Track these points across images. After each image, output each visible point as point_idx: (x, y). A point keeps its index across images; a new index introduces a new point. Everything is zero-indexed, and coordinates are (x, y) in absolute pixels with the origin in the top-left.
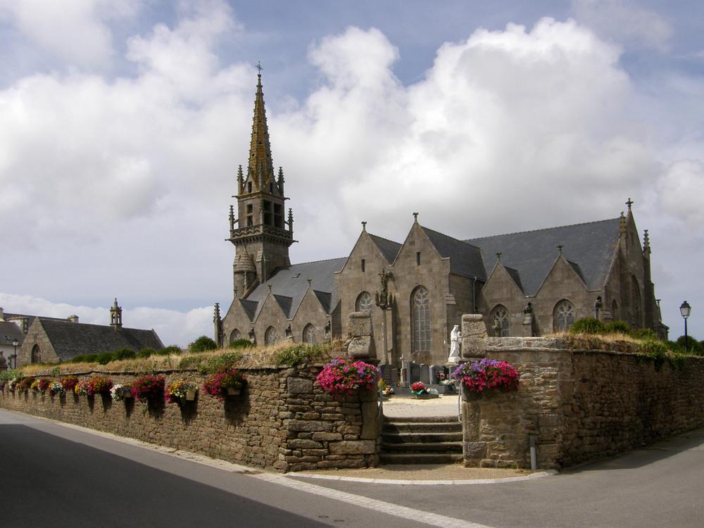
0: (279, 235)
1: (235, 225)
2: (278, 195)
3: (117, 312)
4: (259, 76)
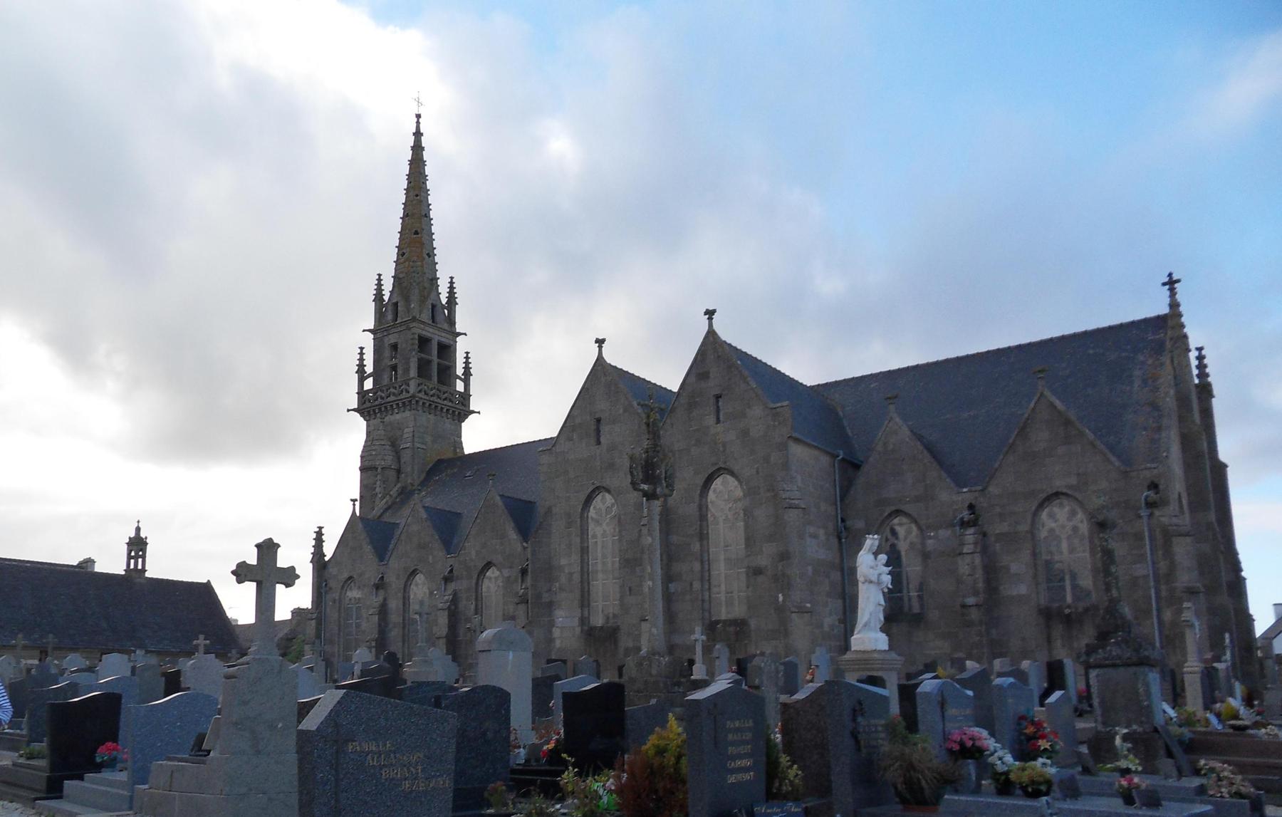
0: (445, 399)
1: (365, 382)
2: (446, 326)
3: (137, 545)
4: (418, 116)
